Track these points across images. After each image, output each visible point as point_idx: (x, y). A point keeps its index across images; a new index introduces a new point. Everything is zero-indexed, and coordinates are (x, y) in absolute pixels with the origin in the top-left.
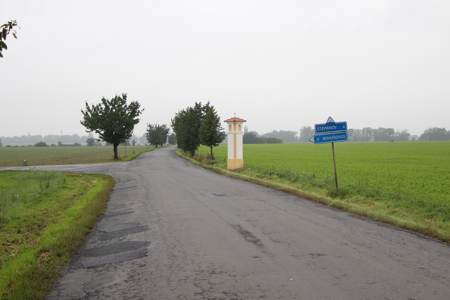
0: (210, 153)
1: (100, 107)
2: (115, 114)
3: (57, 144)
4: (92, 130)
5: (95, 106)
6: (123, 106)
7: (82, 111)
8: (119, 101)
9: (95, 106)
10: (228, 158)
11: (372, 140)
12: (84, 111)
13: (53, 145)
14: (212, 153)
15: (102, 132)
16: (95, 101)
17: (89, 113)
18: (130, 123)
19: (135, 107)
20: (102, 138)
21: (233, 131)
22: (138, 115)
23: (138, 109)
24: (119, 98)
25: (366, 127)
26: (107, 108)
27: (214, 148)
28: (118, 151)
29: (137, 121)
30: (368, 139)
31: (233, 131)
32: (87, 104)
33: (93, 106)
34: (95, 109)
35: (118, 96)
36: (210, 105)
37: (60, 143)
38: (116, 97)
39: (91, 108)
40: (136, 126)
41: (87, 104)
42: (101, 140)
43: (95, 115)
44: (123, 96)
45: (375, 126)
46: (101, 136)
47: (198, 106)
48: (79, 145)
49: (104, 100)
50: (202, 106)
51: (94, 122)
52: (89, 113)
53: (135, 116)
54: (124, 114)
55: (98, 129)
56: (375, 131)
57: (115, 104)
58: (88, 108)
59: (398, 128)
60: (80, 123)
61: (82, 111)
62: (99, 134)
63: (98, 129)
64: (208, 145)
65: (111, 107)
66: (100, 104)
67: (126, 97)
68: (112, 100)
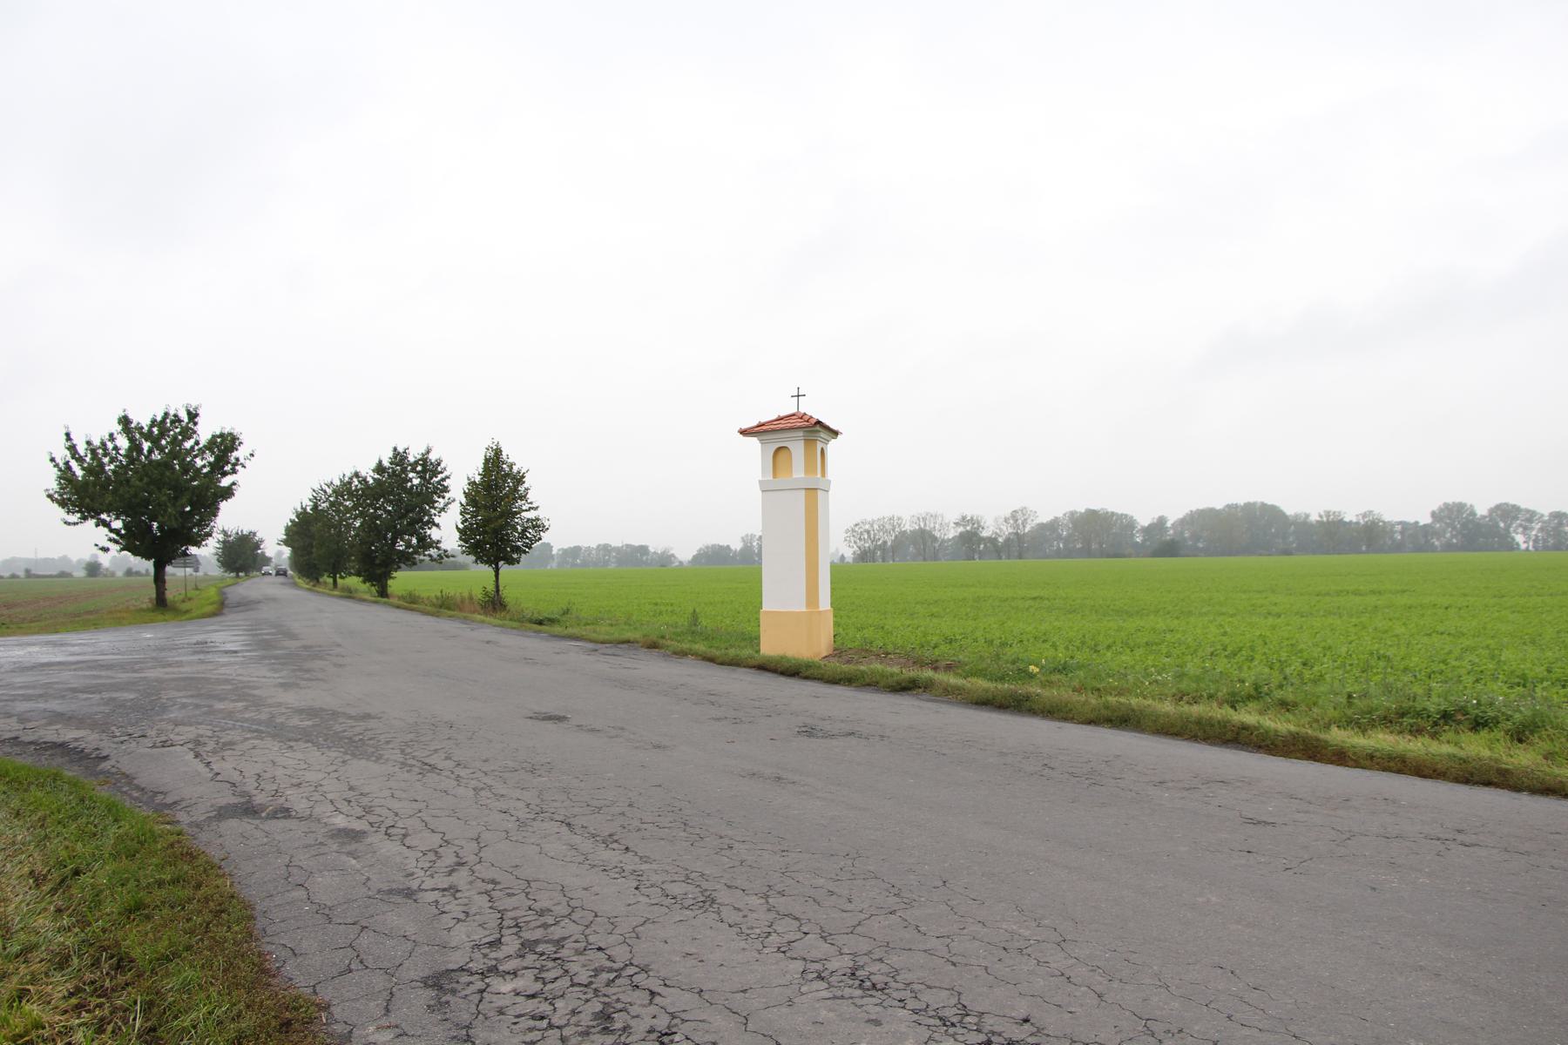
0: (491, 587)
1: (110, 446)
2: (165, 465)
3: (22, 574)
4: (84, 518)
5: (97, 443)
6: (188, 444)
7: (53, 460)
8: (172, 430)
9: (97, 443)
10: (767, 606)
11: (612, 566)
12: (58, 460)
13: (13, 576)
14: (497, 586)
15: (118, 524)
16: (97, 426)
17: (74, 464)
18: (209, 497)
19: (225, 445)
20: (116, 542)
21: (798, 472)
22: (234, 471)
23: (235, 454)
24: (177, 420)
25: (602, 542)
26: (135, 447)
27: (505, 569)
28: (168, 585)
29: (228, 493)
30: (606, 563)
31: (798, 472)
32: (68, 435)
33: (89, 443)
34: (94, 452)
35: (172, 412)
36: (433, 457)
37: (27, 571)
38: (166, 414)
39: (82, 449)
40: (223, 505)
41: (68, 435)
42: (114, 547)
43: (95, 470)
44: (189, 413)
45: (616, 542)
46: (113, 536)
47: (399, 458)
48: (69, 575)
49: (125, 421)
50: (411, 459)
51: (91, 489)
52: (74, 464)
53: (225, 474)
54: (187, 468)
55: (104, 516)
56: (617, 550)
57: (162, 434)
58: (73, 449)
59: (656, 545)
60: (44, 495)
61: (53, 460)
62: (106, 530)
63: (104, 516)
64: (489, 562)
65: (146, 445)
66: (111, 435)
67: (197, 415)
68: (153, 423)
